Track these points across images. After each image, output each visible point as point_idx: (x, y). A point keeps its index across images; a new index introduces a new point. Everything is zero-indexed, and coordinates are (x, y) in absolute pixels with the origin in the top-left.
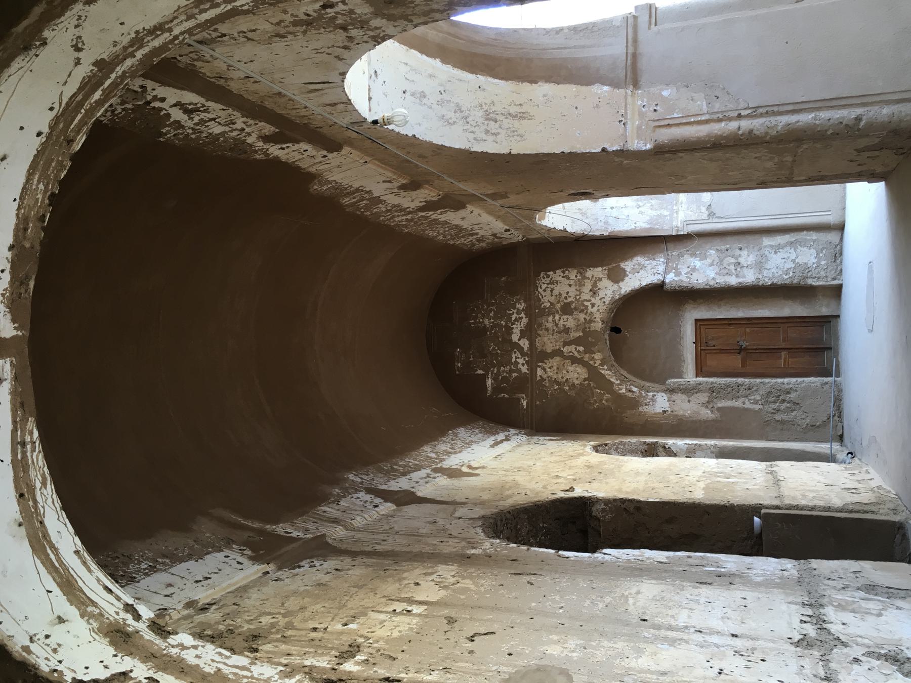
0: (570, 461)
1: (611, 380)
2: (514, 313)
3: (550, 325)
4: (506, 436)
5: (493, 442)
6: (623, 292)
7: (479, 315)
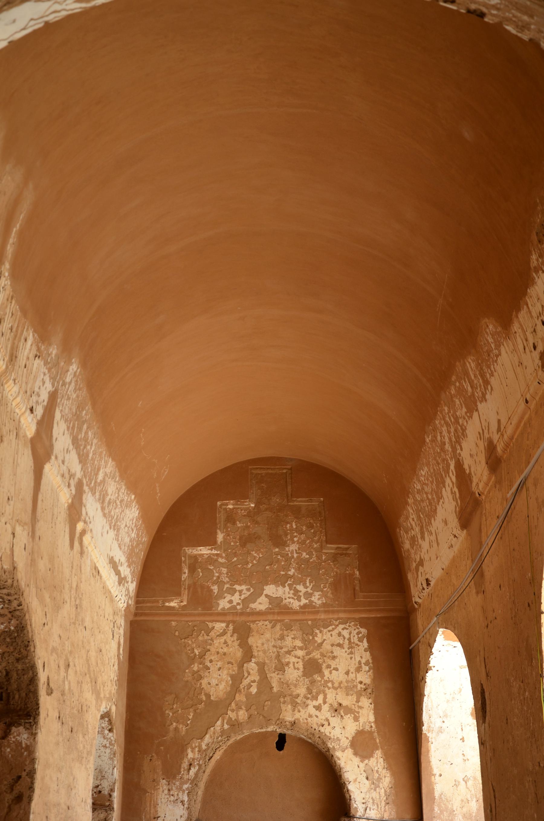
0: (89, 680)
1: (207, 736)
2: (306, 587)
3: (288, 642)
4: (125, 578)
5: (117, 561)
6: (338, 754)
7: (303, 537)
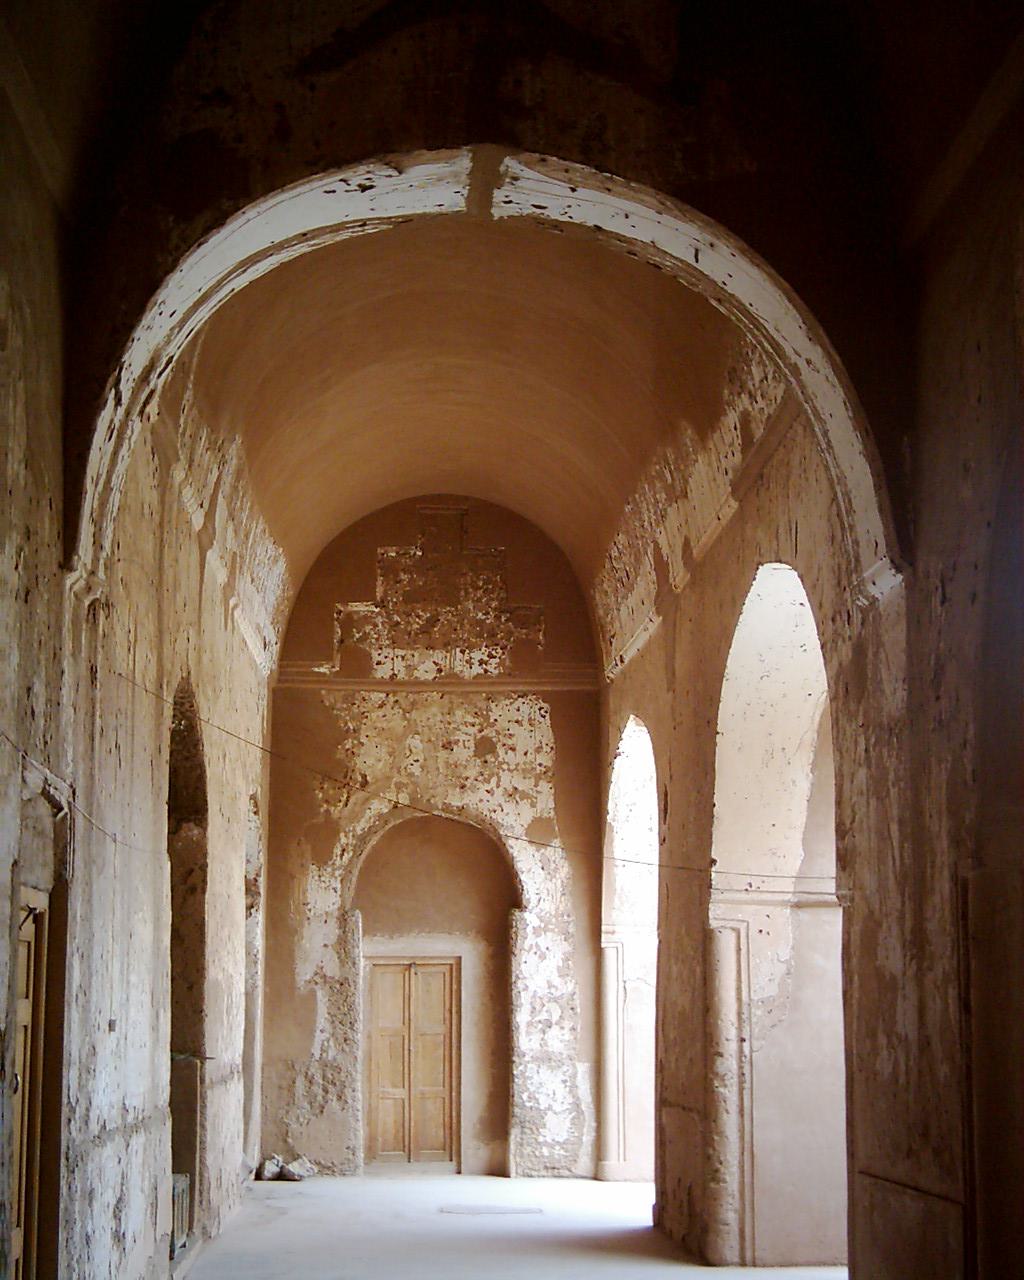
6: (511, 842)
